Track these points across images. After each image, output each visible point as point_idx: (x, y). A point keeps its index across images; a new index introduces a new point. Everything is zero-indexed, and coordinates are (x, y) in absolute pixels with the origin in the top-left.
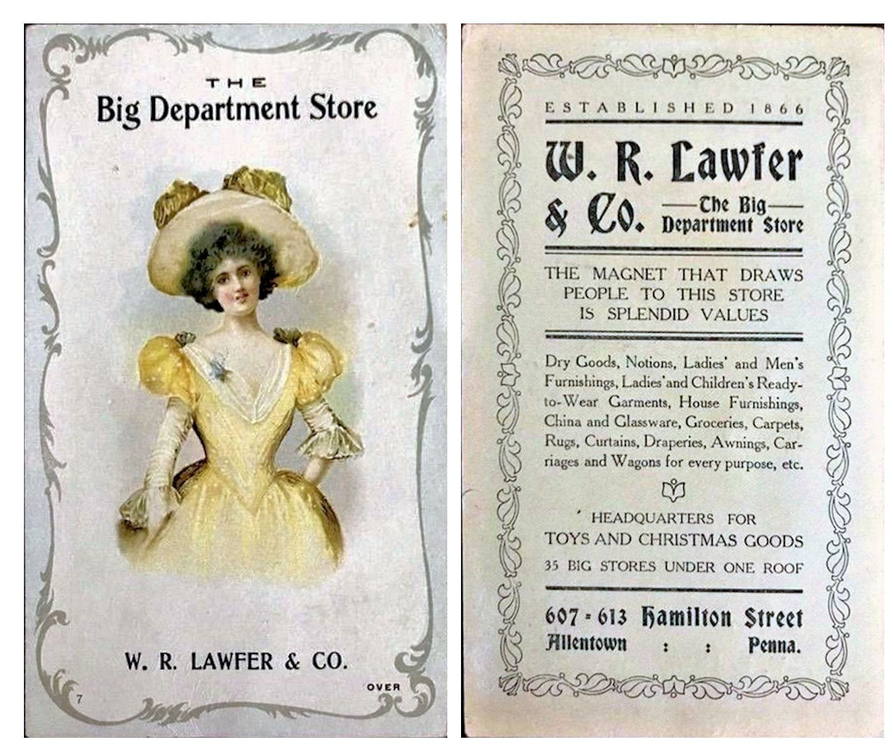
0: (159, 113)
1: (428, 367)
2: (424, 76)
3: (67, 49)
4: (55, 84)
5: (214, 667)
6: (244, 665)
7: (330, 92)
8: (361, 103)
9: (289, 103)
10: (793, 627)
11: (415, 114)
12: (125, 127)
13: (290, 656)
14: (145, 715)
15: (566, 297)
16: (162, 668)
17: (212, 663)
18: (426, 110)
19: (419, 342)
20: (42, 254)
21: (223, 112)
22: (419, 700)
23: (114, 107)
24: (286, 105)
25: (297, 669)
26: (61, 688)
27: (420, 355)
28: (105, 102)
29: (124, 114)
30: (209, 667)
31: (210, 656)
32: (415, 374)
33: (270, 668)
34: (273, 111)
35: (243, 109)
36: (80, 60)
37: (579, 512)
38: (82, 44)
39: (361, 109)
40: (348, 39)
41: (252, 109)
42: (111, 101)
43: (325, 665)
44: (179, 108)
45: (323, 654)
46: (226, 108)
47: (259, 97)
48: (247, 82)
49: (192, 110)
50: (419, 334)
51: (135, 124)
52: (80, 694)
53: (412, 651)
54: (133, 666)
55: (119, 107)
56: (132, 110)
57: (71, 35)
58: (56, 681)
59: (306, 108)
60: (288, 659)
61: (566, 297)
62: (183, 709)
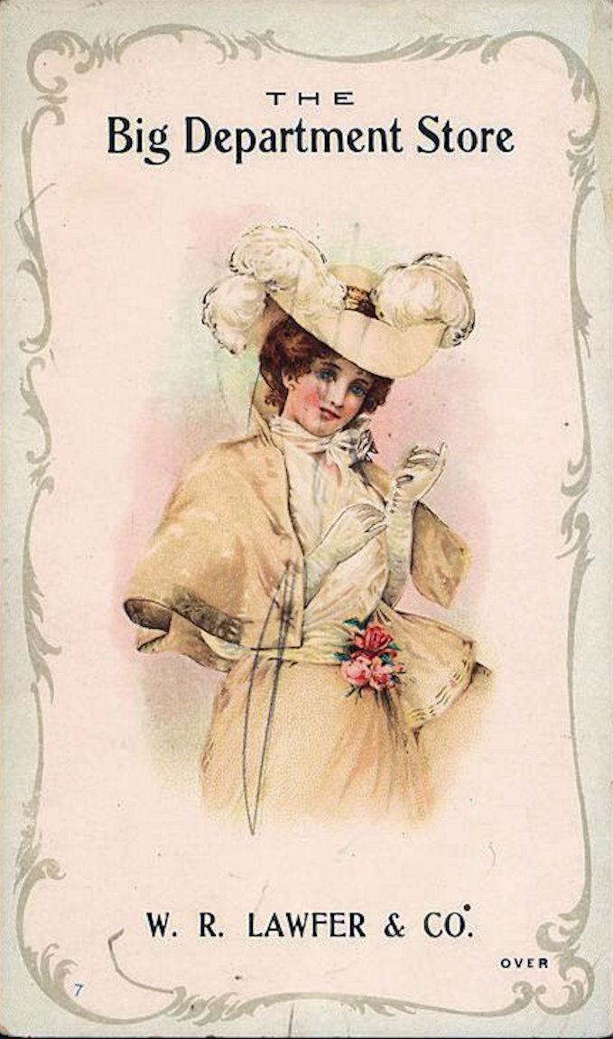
0: (198, 142)
1: (583, 516)
2: (582, 98)
3: (62, 52)
4: (45, 103)
5: (281, 934)
6: (323, 930)
8: (492, 132)
9: (387, 129)
11: (568, 153)
12: (148, 161)
13: (391, 918)
14: (174, 1010)
16: (203, 934)
17: (278, 928)
18: (585, 148)
19: (572, 481)
20: (25, 348)
21: (292, 140)
22: (572, 990)
25: (400, 935)
26: (52, 975)
27: (575, 498)
28: (119, 126)
29: (146, 143)
30: (274, 934)
31: (275, 918)
32: (567, 527)
33: (362, 935)
34: (364, 140)
35: (321, 137)
36: (82, 69)
38: (84, 46)
39: (491, 139)
40: (471, 45)
41: (334, 136)
42: (127, 124)
43: (441, 932)
44: (228, 134)
45: (439, 915)
46: (296, 134)
47: (344, 120)
48: (327, 99)
49: (245, 136)
50: (572, 470)
51: (163, 157)
52: (80, 983)
53: (561, 922)
54: (158, 929)
55: (139, 132)
56: (158, 137)
57: (72, 35)
58: (46, 960)
59: (410, 137)
60: (389, 922)
62: (230, 1002)
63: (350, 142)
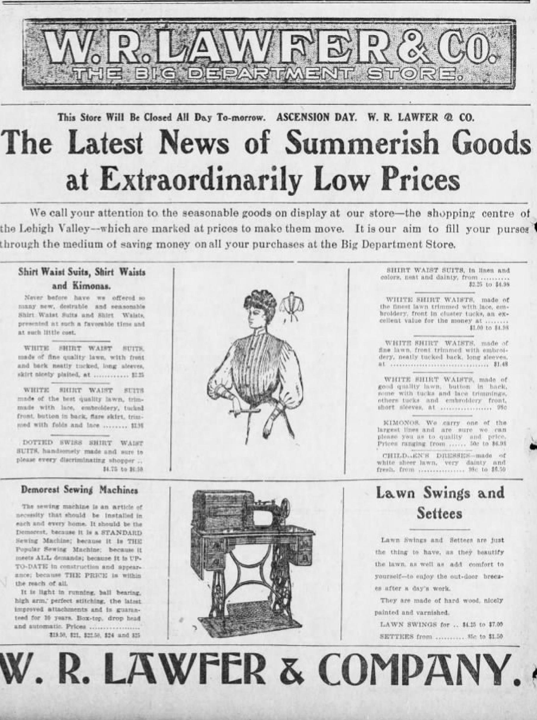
28: (345, 242)
30: (141, 680)
45: (339, 655)
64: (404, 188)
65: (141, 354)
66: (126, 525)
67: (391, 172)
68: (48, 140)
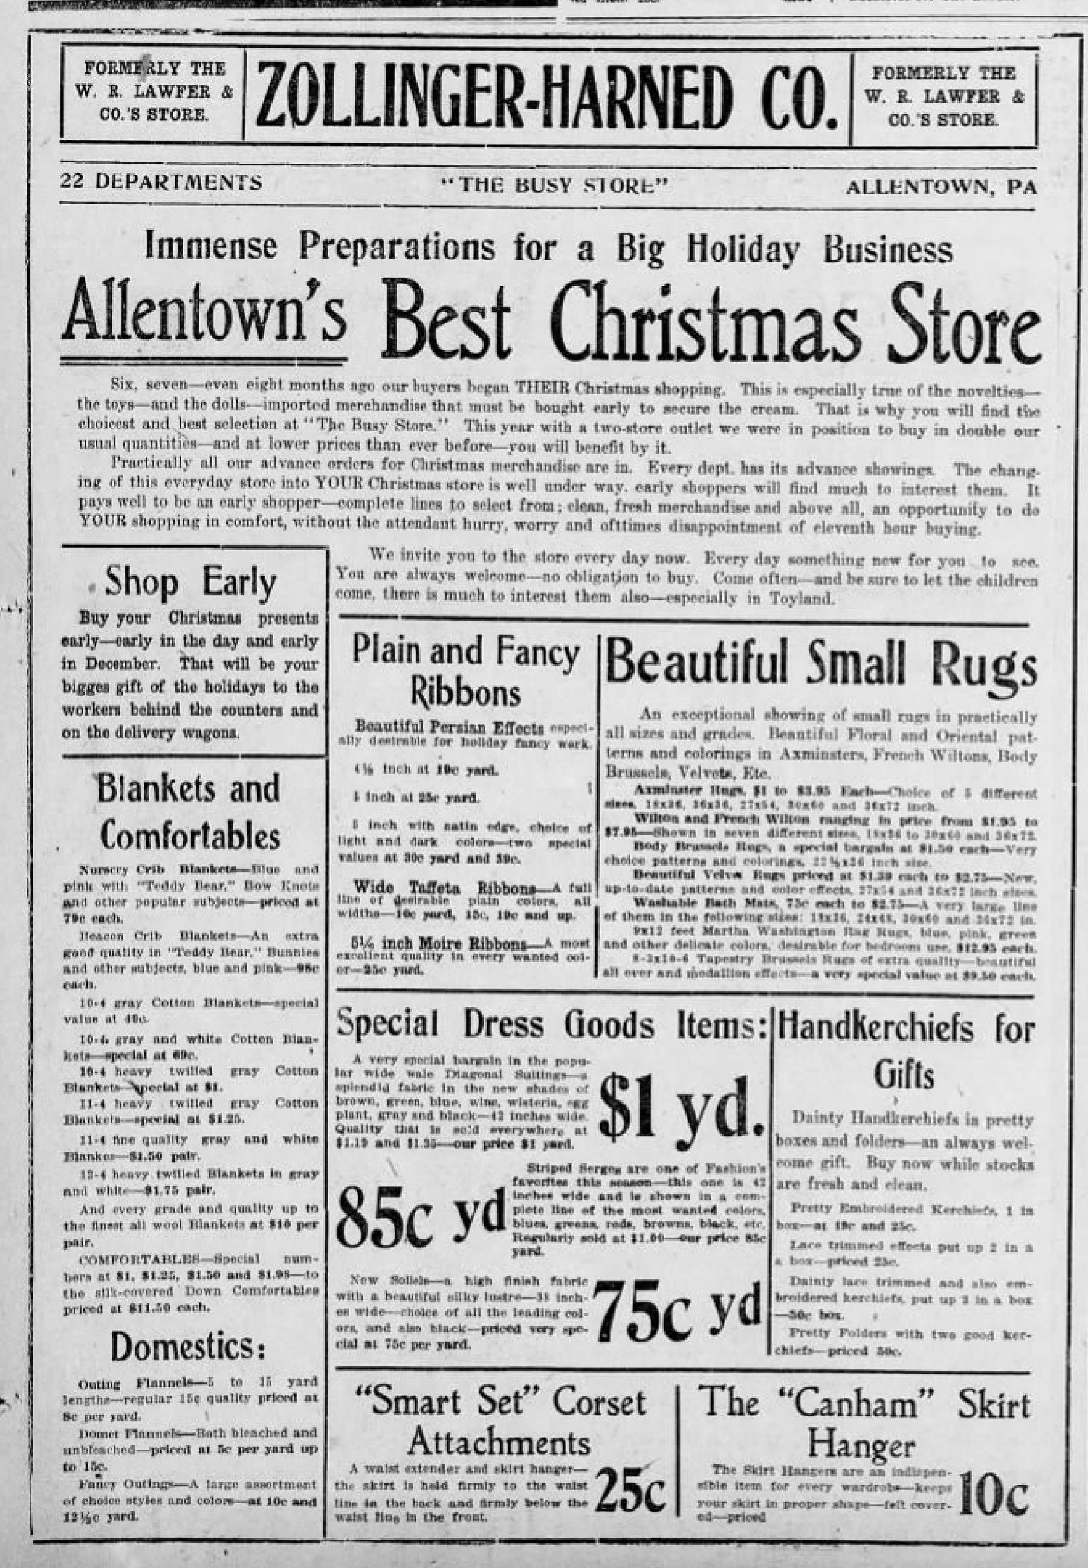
7: (465, 379)
8: (892, 1023)
10: (203, 339)
12: (992, 695)
15: (304, 256)
21: (199, 839)
23: (636, 245)
24: (156, 833)
28: (627, 240)
29: (990, 674)
37: (13, 473)
41: (171, 1348)
42: (632, 238)
44: (878, 1025)
46: (451, 1401)
55: (642, 245)
56: (1004, 666)
61: (304, 256)
63: (871, 1032)
64: (325, 255)
65: (1025, 1156)
66: (192, 1088)
67: (310, 238)
68: (273, 241)
